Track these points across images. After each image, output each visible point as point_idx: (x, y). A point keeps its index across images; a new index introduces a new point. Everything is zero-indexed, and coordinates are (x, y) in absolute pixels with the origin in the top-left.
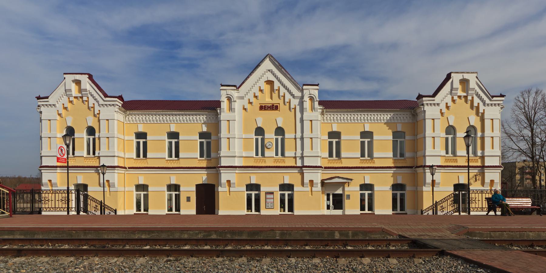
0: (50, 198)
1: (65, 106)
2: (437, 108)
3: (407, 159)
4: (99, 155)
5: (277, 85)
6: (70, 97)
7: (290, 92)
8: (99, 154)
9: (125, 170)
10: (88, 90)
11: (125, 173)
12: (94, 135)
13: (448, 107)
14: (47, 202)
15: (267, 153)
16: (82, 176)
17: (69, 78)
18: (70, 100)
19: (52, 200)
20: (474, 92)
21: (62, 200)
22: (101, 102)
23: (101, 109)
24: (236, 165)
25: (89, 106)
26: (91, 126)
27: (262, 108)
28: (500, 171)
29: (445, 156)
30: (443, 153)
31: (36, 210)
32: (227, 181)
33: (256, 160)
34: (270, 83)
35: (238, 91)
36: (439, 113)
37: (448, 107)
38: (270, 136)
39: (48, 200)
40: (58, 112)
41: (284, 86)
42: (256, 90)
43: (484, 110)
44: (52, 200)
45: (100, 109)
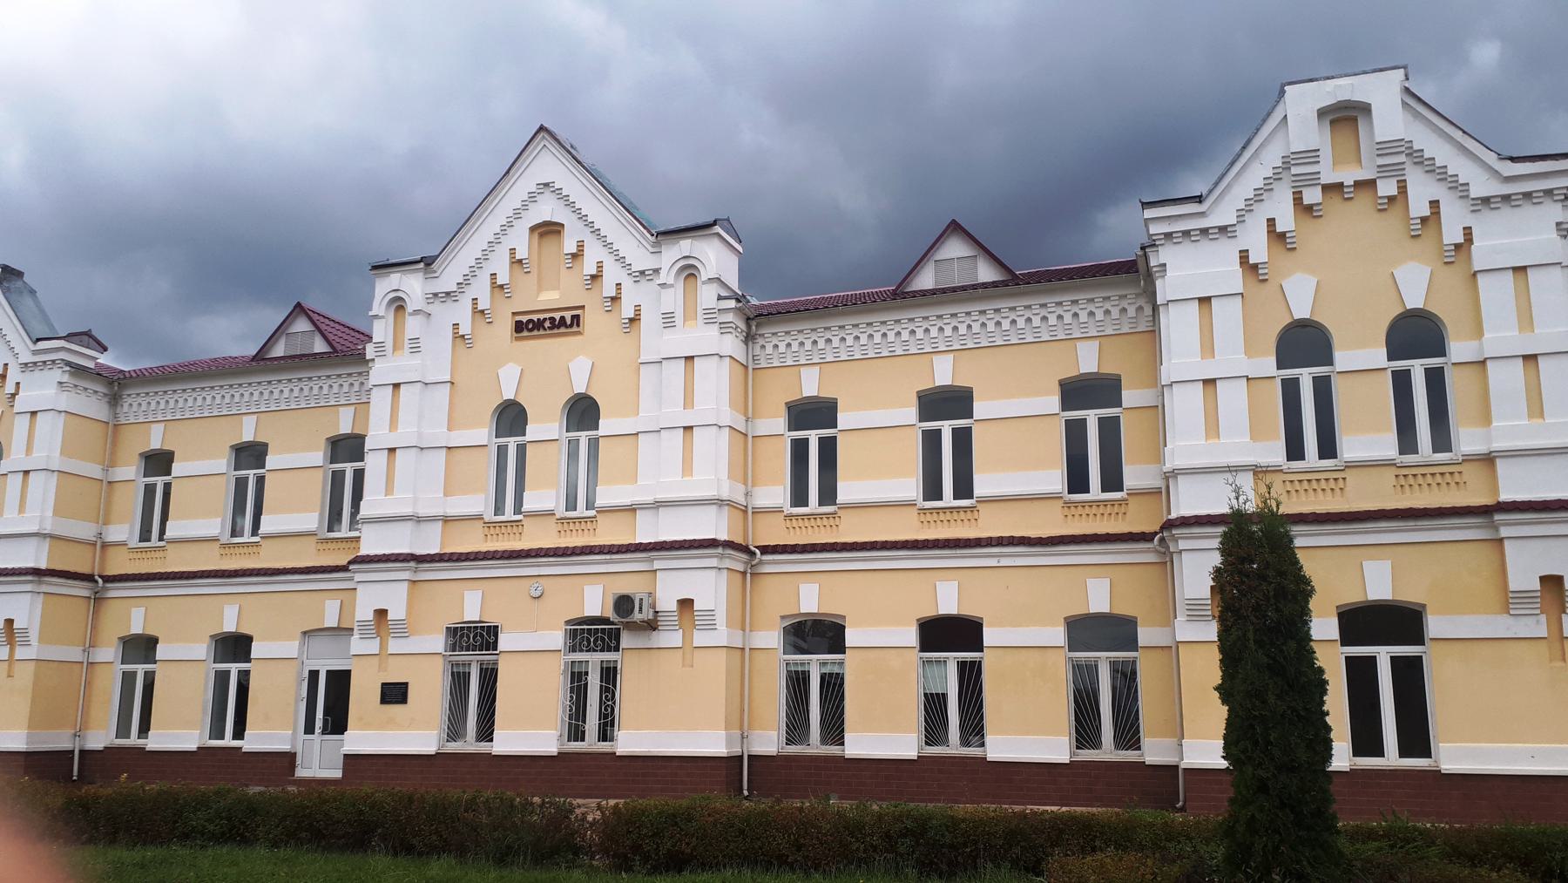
15: (1351, 447)
16: (1387, 565)
28: (1215, 543)
30: (1274, 452)
32: (1544, 579)
36: (1236, 267)
38: (546, 426)
43: (1468, 231)
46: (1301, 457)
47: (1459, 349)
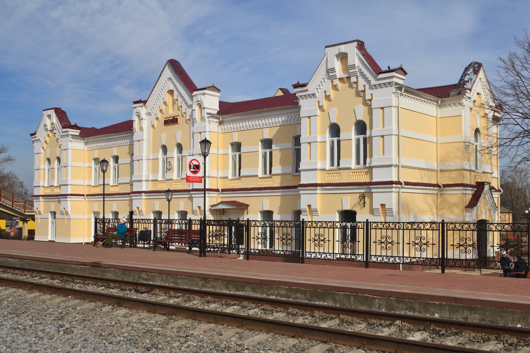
0: (395, 239)
1: (327, 95)
2: (314, 101)
4: (371, 165)
5: (176, 93)
6: (334, 80)
8: (371, 163)
9: (399, 186)
10: (356, 65)
11: (400, 192)
12: (365, 134)
13: (328, 97)
14: (425, 246)
17: (333, 52)
18: (334, 84)
19: (433, 244)
21: (382, 243)
22: (373, 82)
23: (374, 92)
24: (319, 182)
25: (359, 90)
26: (335, 123)
31: (404, 262)
35: (146, 107)
39: (391, 243)
40: (319, 103)
42: (160, 103)
44: (433, 244)
45: (372, 92)
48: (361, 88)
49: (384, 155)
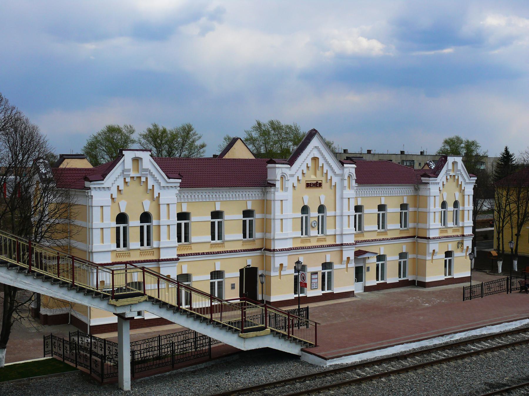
2: (107, 194)
3: (410, 230)
5: (321, 162)
7: (332, 169)
20: (148, 173)
22: (163, 184)
23: (161, 192)
27: (308, 185)
29: (115, 251)
30: (114, 247)
33: (118, 255)
34: (315, 159)
36: (110, 199)
37: (119, 191)
41: (328, 163)
42: (304, 168)
46: (214, 240)
47: (154, 222)
48: (150, 187)
49: (469, 220)
